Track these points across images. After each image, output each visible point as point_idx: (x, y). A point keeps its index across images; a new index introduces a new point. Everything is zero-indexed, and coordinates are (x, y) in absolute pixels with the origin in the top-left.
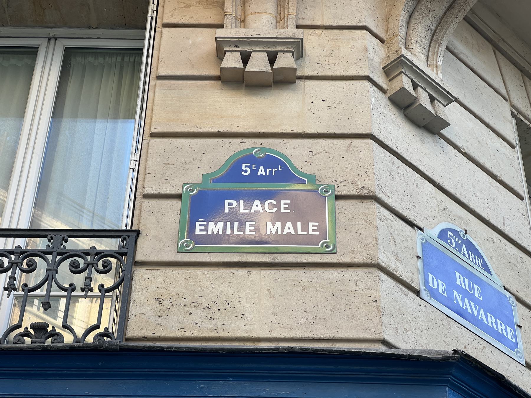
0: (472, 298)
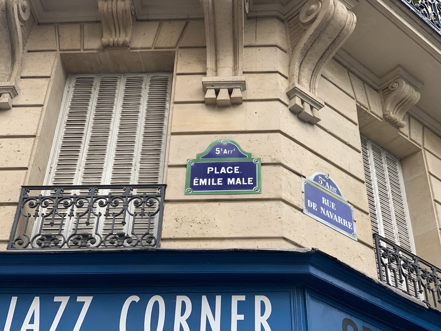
0: (330, 209)
